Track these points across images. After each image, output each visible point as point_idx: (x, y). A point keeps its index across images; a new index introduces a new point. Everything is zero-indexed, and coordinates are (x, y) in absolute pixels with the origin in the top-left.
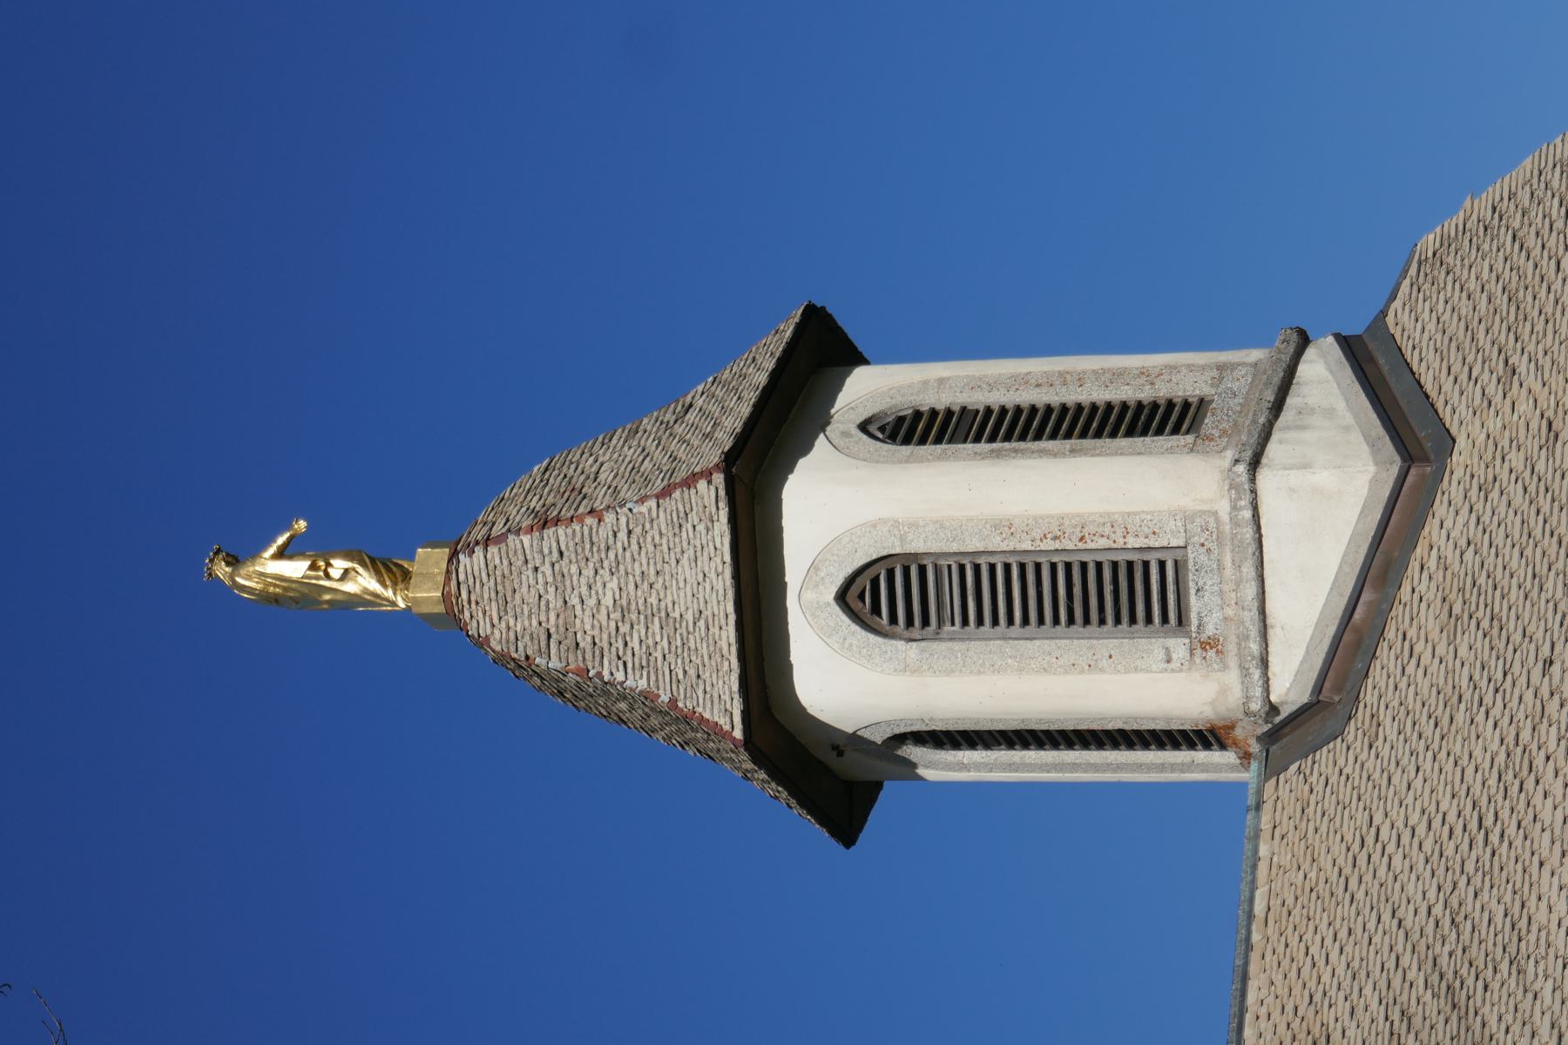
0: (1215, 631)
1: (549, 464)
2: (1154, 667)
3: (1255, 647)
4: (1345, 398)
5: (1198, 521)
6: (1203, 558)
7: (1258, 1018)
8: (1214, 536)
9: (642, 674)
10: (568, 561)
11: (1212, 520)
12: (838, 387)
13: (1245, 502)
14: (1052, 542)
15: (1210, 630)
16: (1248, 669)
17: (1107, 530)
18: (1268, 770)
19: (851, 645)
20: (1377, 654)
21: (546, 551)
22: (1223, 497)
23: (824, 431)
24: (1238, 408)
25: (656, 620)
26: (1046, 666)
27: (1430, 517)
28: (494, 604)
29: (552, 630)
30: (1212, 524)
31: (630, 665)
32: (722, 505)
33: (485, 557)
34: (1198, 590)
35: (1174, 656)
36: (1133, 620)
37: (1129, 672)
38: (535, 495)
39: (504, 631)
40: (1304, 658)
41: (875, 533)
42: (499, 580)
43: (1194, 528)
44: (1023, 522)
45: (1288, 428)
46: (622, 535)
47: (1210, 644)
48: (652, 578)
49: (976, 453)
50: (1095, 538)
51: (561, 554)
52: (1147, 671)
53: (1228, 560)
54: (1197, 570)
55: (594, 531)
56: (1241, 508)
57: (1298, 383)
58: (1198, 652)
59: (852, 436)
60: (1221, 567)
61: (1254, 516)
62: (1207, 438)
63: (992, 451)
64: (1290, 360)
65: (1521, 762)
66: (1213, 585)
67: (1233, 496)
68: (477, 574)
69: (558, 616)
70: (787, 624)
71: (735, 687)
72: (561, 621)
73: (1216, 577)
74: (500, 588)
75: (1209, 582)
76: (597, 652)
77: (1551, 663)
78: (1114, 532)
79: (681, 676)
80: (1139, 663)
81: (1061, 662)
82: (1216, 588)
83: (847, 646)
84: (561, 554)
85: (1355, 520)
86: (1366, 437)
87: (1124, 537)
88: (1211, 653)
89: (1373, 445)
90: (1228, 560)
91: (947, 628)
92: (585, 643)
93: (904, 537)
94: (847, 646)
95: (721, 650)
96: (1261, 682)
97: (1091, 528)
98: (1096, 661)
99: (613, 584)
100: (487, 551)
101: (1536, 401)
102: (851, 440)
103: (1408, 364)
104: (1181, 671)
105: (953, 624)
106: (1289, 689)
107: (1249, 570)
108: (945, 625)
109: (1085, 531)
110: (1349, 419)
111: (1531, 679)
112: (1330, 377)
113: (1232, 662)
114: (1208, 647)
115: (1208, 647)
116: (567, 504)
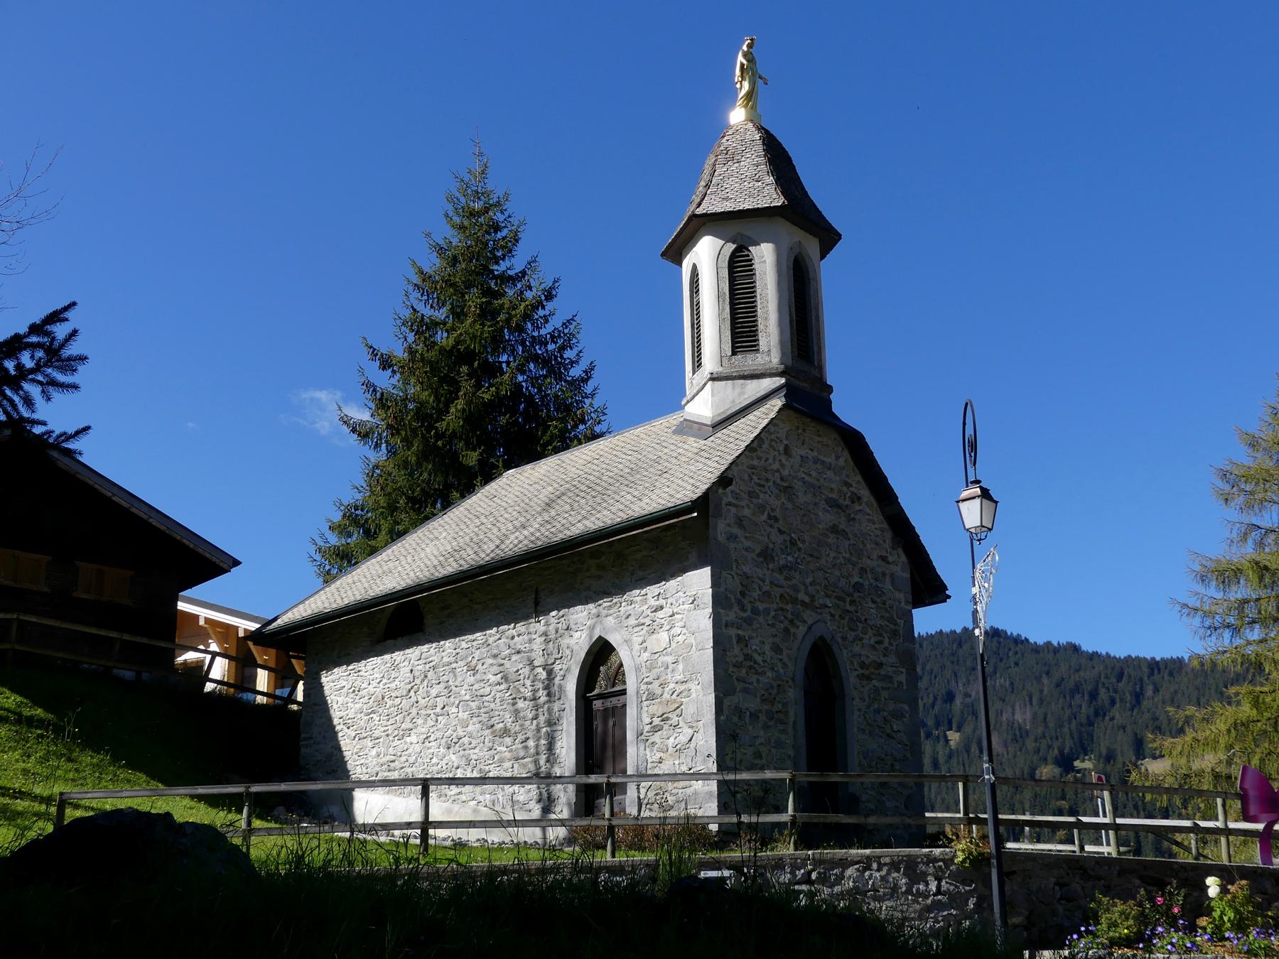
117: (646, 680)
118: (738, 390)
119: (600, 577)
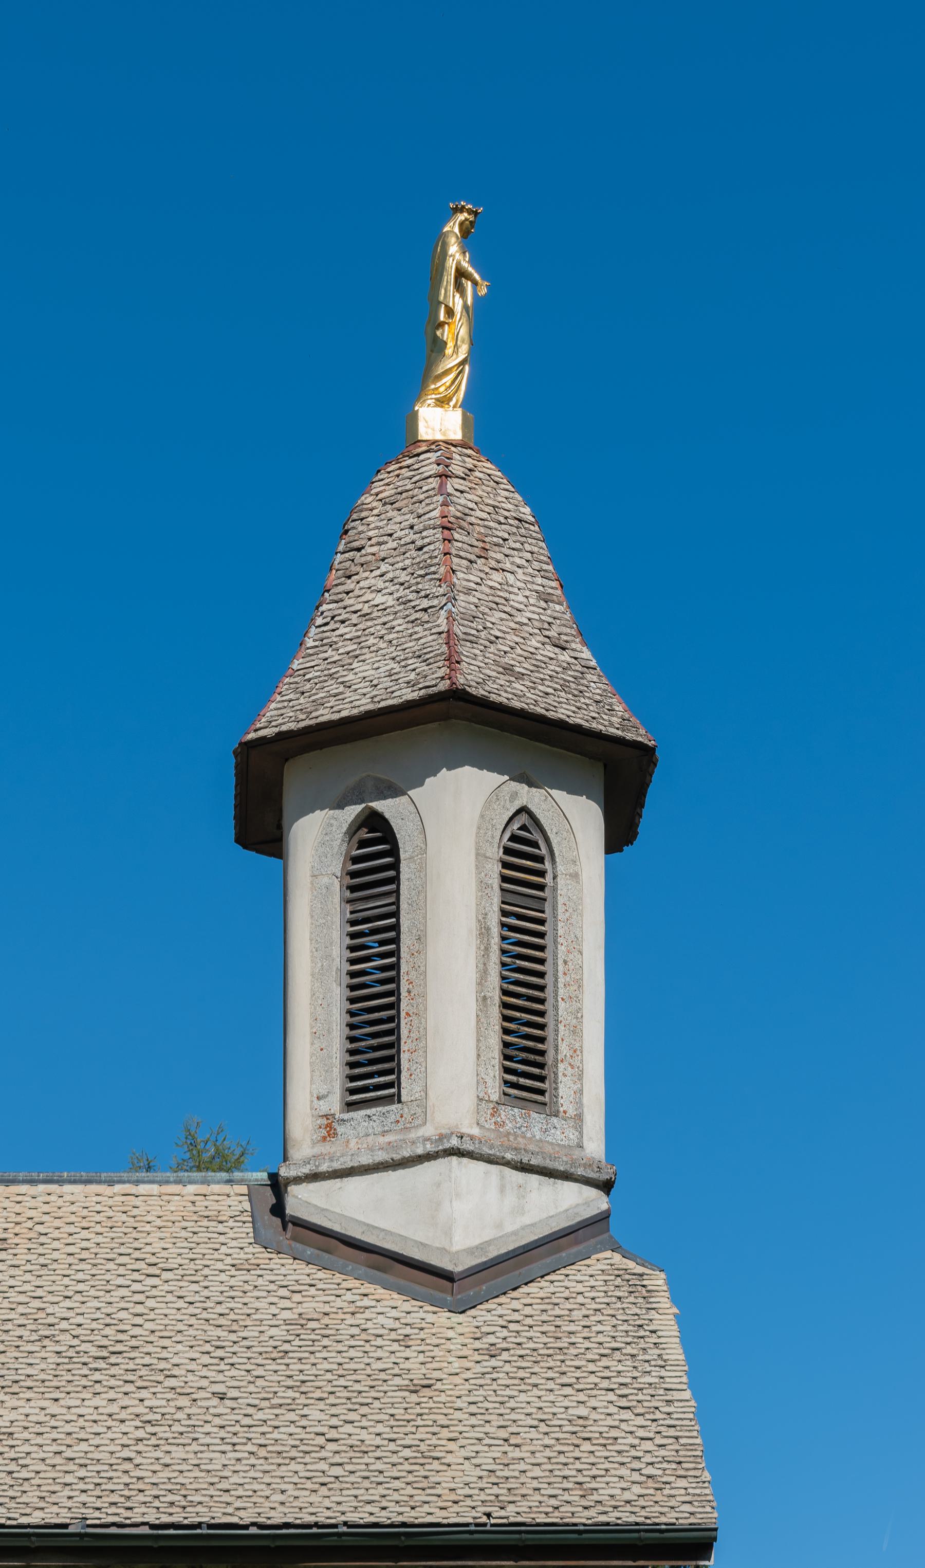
0: (340, 1133)
1: (526, 522)
2: (314, 1086)
3: (324, 1167)
4: (536, 1224)
5: (419, 1110)
6: (393, 1118)
7: (49, 1194)
8: (408, 1125)
9: (317, 640)
10: (415, 555)
11: (419, 1122)
13: (429, 1147)
14: (406, 989)
15: (340, 1129)
16: (309, 1164)
17: (414, 1035)
18: (256, 1186)
19: (332, 825)
20: (310, 1266)
21: (424, 534)
22: (436, 1129)
23: (510, 779)
24: (529, 1135)
25: (355, 646)
26: (316, 995)
27: (405, 1298)
28: (393, 492)
29: (363, 552)
30: (417, 1122)
31: (325, 628)
32: (422, 692)
33: (430, 477)
34: (369, 1116)
35: (321, 1102)
36: (352, 1065)
37: (311, 1066)
38: (489, 513)
39: (370, 506)
40: (319, 1207)
41: (416, 834)
42: (410, 493)
43: (414, 1109)
44: (421, 963)
45: (502, 1177)
46: (425, 603)
47: (330, 1130)
48: (386, 638)
49: (486, 914)
50: (408, 1026)
51: (420, 549)
52: (311, 1081)
53: (390, 1138)
54: (384, 1114)
55: (434, 576)
56: (424, 1145)
57: (563, 1184)
58: (325, 1121)
59: (511, 802)
60: (384, 1133)
61: (420, 1156)
62: (494, 1112)
63: (488, 929)
64: (579, 1175)
65: (150, 1381)
66: (373, 1128)
67: (434, 1138)
68: (420, 471)
69: (374, 554)
71: (284, 728)
72: (369, 558)
73: (379, 1129)
74: (404, 495)
75: (376, 1126)
76: (340, 596)
77: (222, 1399)
78: (412, 1041)
79: (307, 677)
80: (317, 1073)
81: (319, 1009)
82: (370, 1131)
83: (332, 821)
84: (420, 549)
85: (416, 1239)
86: (489, 1243)
87: (409, 1051)
88: (324, 1132)
89: (481, 1248)
90: (390, 1138)
91: (349, 908)
92: (350, 585)
93: (412, 860)
94: (332, 821)
95: (316, 710)
96: (300, 1174)
97: (415, 1022)
98: (319, 1038)
99: (390, 601)
100: (435, 477)
101: (457, 1374)
102: (508, 802)
103: (554, 1271)
104: (311, 1109)
105: (351, 913)
106: (297, 1197)
107: (381, 1156)
108: (350, 905)
109: (414, 1017)
110: (509, 1228)
111: (217, 1384)
112: (561, 1209)
114: (328, 1129)
115: (328, 1129)
116: (465, 546)
118: (511, 1199)
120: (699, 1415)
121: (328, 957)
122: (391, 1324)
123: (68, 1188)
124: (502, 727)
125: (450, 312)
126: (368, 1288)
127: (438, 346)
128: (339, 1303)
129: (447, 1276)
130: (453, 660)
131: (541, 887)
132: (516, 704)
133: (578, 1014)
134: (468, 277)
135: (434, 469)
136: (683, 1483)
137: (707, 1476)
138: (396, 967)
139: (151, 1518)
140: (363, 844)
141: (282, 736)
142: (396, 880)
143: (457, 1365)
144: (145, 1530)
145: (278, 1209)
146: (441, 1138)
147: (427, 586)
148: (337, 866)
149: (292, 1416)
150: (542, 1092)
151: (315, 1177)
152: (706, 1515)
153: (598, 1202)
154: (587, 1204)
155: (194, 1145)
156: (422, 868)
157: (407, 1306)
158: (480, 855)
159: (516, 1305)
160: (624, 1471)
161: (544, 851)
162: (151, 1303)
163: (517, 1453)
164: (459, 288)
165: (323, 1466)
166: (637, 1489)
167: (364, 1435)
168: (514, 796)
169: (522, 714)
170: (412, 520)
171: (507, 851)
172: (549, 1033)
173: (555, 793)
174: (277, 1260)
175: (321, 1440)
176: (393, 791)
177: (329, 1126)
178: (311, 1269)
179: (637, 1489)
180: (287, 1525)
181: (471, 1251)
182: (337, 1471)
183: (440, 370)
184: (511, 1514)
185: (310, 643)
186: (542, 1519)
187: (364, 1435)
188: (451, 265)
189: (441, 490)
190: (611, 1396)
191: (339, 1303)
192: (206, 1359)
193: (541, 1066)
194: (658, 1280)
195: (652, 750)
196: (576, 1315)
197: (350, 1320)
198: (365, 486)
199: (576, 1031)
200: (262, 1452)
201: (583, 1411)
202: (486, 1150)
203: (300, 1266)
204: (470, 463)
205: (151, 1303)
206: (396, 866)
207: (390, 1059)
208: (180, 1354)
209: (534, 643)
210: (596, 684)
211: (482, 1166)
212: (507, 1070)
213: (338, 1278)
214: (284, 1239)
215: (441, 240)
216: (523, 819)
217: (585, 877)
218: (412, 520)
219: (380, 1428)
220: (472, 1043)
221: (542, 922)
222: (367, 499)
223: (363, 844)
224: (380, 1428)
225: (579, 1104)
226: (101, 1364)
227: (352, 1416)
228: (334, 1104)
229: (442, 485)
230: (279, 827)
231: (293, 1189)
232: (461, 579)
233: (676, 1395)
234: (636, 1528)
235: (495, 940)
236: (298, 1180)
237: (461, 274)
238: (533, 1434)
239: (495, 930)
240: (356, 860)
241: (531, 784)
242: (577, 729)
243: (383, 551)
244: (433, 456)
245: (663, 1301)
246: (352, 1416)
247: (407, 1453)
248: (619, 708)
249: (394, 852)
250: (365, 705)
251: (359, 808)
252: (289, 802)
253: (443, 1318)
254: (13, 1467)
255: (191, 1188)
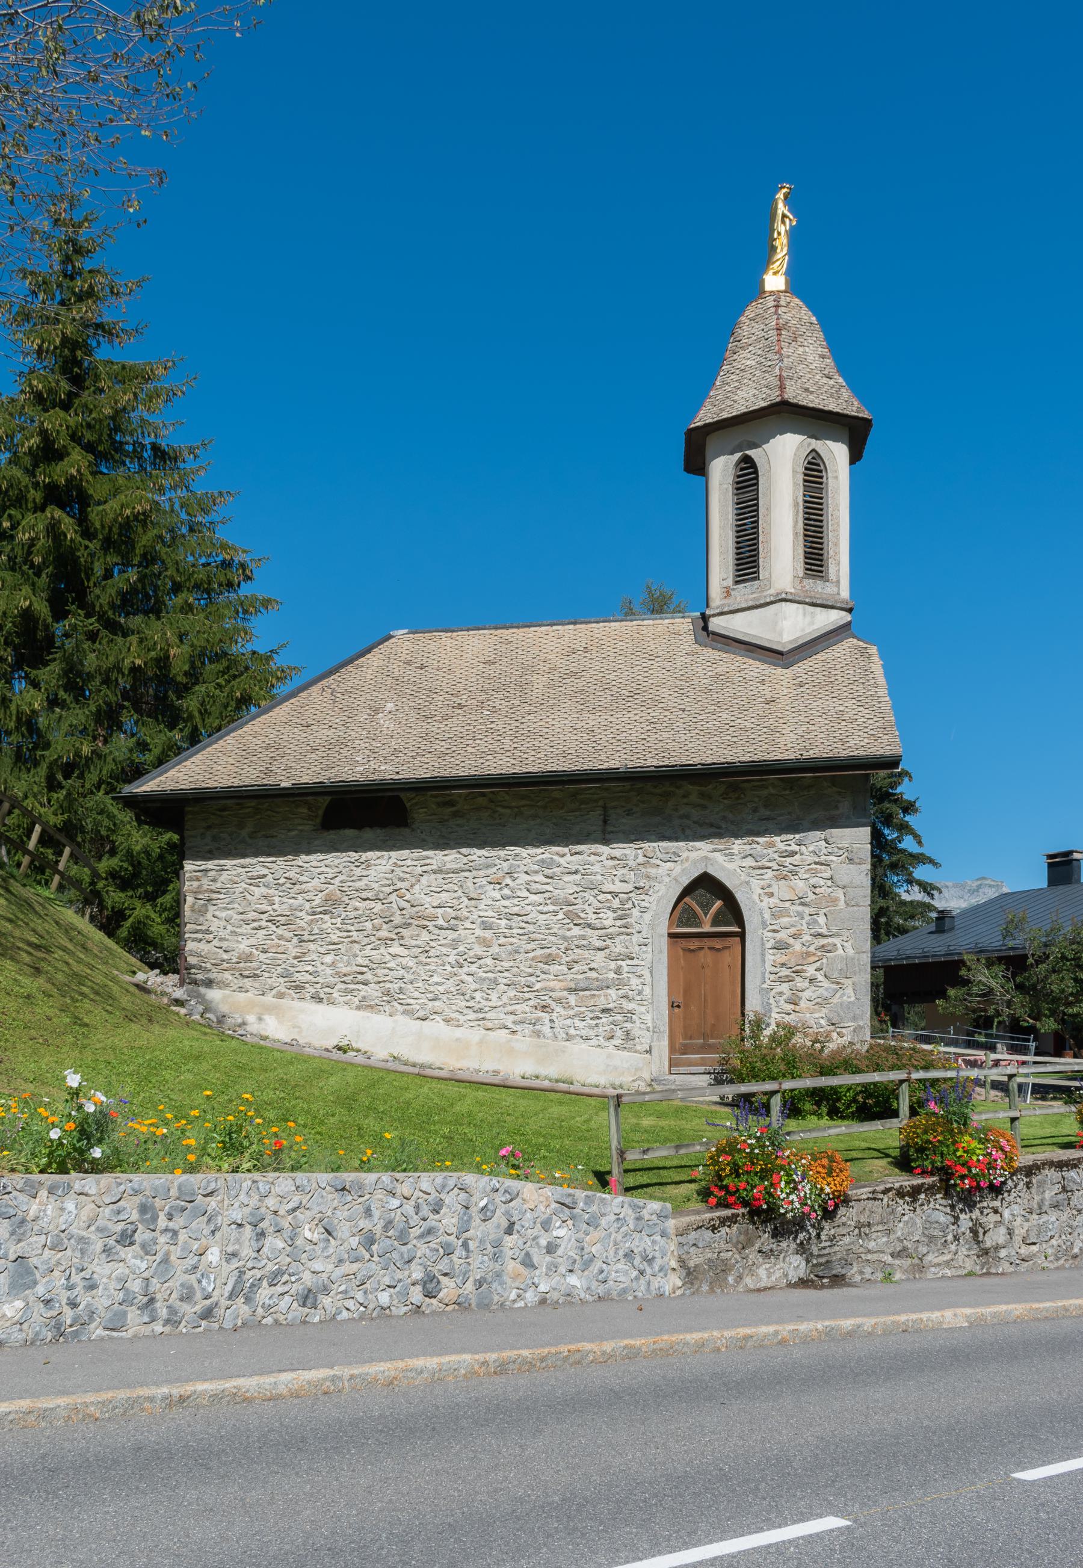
12: (835, 440)
13: (772, 599)
15: (733, 593)
36: (738, 565)
43: (766, 582)
46: (769, 363)
53: (755, 595)
70: (795, 433)
75: (748, 590)
89: (795, 640)
90: (755, 595)
92: (735, 357)
99: (754, 363)
107: (751, 603)
110: (807, 631)
113: (723, 602)
117: (771, 927)
118: (808, 619)
119: (704, 807)
120: (893, 707)
121: (727, 519)
122: (756, 675)
123: (613, 624)
124: (804, 415)
125: (779, 234)
126: (746, 660)
127: (773, 249)
128: (733, 667)
129: (780, 653)
130: (782, 388)
131: (821, 483)
132: (811, 405)
133: (837, 537)
134: (787, 217)
135: (773, 303)
136: (886, 737)
137: (897, 733)
138: (757, 522)
139: (655, 764)
140: (742, 469)
141: (706, 425)
142: (757, 484)
143: (786, 691)
144: (653, 769)
145: (705, 628)
146: (778, 594)
147: (770, 356)
148: (730, 480)
149: (714, 717)
150: (821, 572)
151: (722, 614)
152: (897, 750)
153: (846, 617)
154: (841, 618)
155: (650, 591)
156: (769, 478)
157: (763, 667)
158: (794, 472)
159: (811, 664)
160: (860, 733)
161: (822, 467)
162: (651, 672)
163: (813, 728)
164: (783, 222)
165: (729, 737)
166: (866, 741)
167: (746, 723)
168: (809, 444)
169: (813, 409)
170: (763, 327)
171: (806, 469)
172: (825, 546)
173: (827, 442)
174: (705, 650)
175: (727, 727)
176: (756, 446)
177: (728, 592)
178: (721, 653)
179: (866, 741)
180: (714, 764)
181: (791, 642)
182: (735, 739)
183: (775, 259)
184: (811, 754)
185: (718, 383)
186: (825, 755)
187: (746, 723)
188: (780, 212)
189: (776, 313)
190: (854, 701)
191: (733, 667)
192: (676, 695)
193: (821, 560)
194: (873, 650)
195: (870, 420)
196: (838, 667)
197: (738, 674)
198: (742, 313)
199: (837, 545)
200: (702, 733)
201: (841, 708)
202: (797, 598)
203: (716, 652)
204: (788, 299)
205: (651, 672)
206: (757, 478)
207: (754, 561)
208: (664, 693)
209: (818, 377)
210: (846, 394)
211: (796, 605)
212: (806, 563)
213: (733, 656)
214: (708, 641)
215: (775, 202)
216: (813, 454)
217: (840, 477)
218: (763, 327)
219: (753, 720)
220: (791, 553)
221: (821, 498)
222: (743, 319)
223: (742, 469)
224: (753, 720)
225: (838, 576)
226: (630, 699)
227: (741, 716)
228: (730, 582)
229: (776, 311)
230: (704, 463)
231: (712, 620)
232: (785, 351)
233: (883, 699)
234: (866, 757)
235: (801, 508)
236: (714, 615)
237: (784, 216)
238: (820, 719)
239: (801, 503)
240: (739, 476)
241: (817, 439)
242: (838, 414)
243: (750, 341)
244: (772, 298)
245: (876, 659)
246: (741, 716)
247: (765, 730)
248: (856, 403)
249: (756, 472)
250: (743, 410)
251: (740, 454)
252: (709, 452)
253: (779, 671)
254: (594, 745)
255: (667, 621)
